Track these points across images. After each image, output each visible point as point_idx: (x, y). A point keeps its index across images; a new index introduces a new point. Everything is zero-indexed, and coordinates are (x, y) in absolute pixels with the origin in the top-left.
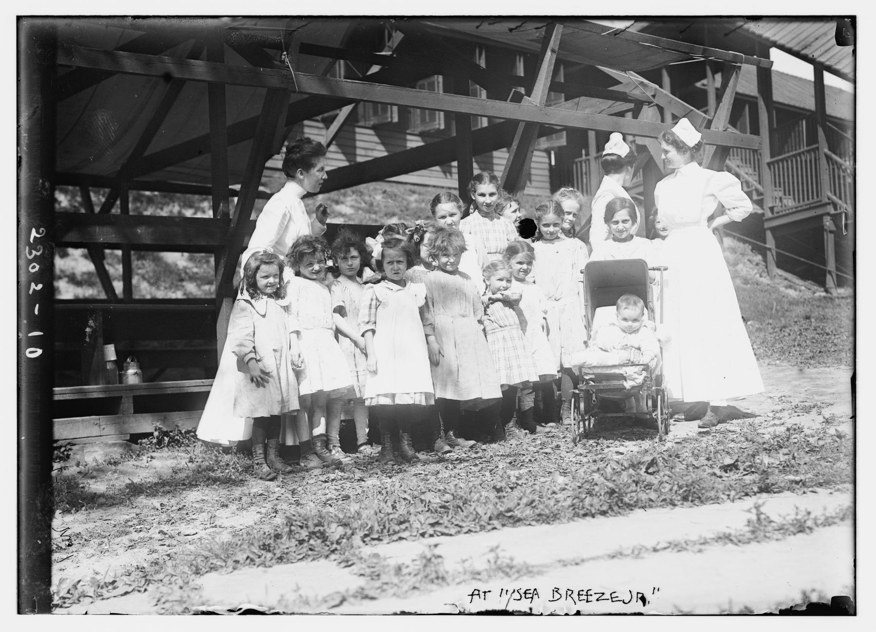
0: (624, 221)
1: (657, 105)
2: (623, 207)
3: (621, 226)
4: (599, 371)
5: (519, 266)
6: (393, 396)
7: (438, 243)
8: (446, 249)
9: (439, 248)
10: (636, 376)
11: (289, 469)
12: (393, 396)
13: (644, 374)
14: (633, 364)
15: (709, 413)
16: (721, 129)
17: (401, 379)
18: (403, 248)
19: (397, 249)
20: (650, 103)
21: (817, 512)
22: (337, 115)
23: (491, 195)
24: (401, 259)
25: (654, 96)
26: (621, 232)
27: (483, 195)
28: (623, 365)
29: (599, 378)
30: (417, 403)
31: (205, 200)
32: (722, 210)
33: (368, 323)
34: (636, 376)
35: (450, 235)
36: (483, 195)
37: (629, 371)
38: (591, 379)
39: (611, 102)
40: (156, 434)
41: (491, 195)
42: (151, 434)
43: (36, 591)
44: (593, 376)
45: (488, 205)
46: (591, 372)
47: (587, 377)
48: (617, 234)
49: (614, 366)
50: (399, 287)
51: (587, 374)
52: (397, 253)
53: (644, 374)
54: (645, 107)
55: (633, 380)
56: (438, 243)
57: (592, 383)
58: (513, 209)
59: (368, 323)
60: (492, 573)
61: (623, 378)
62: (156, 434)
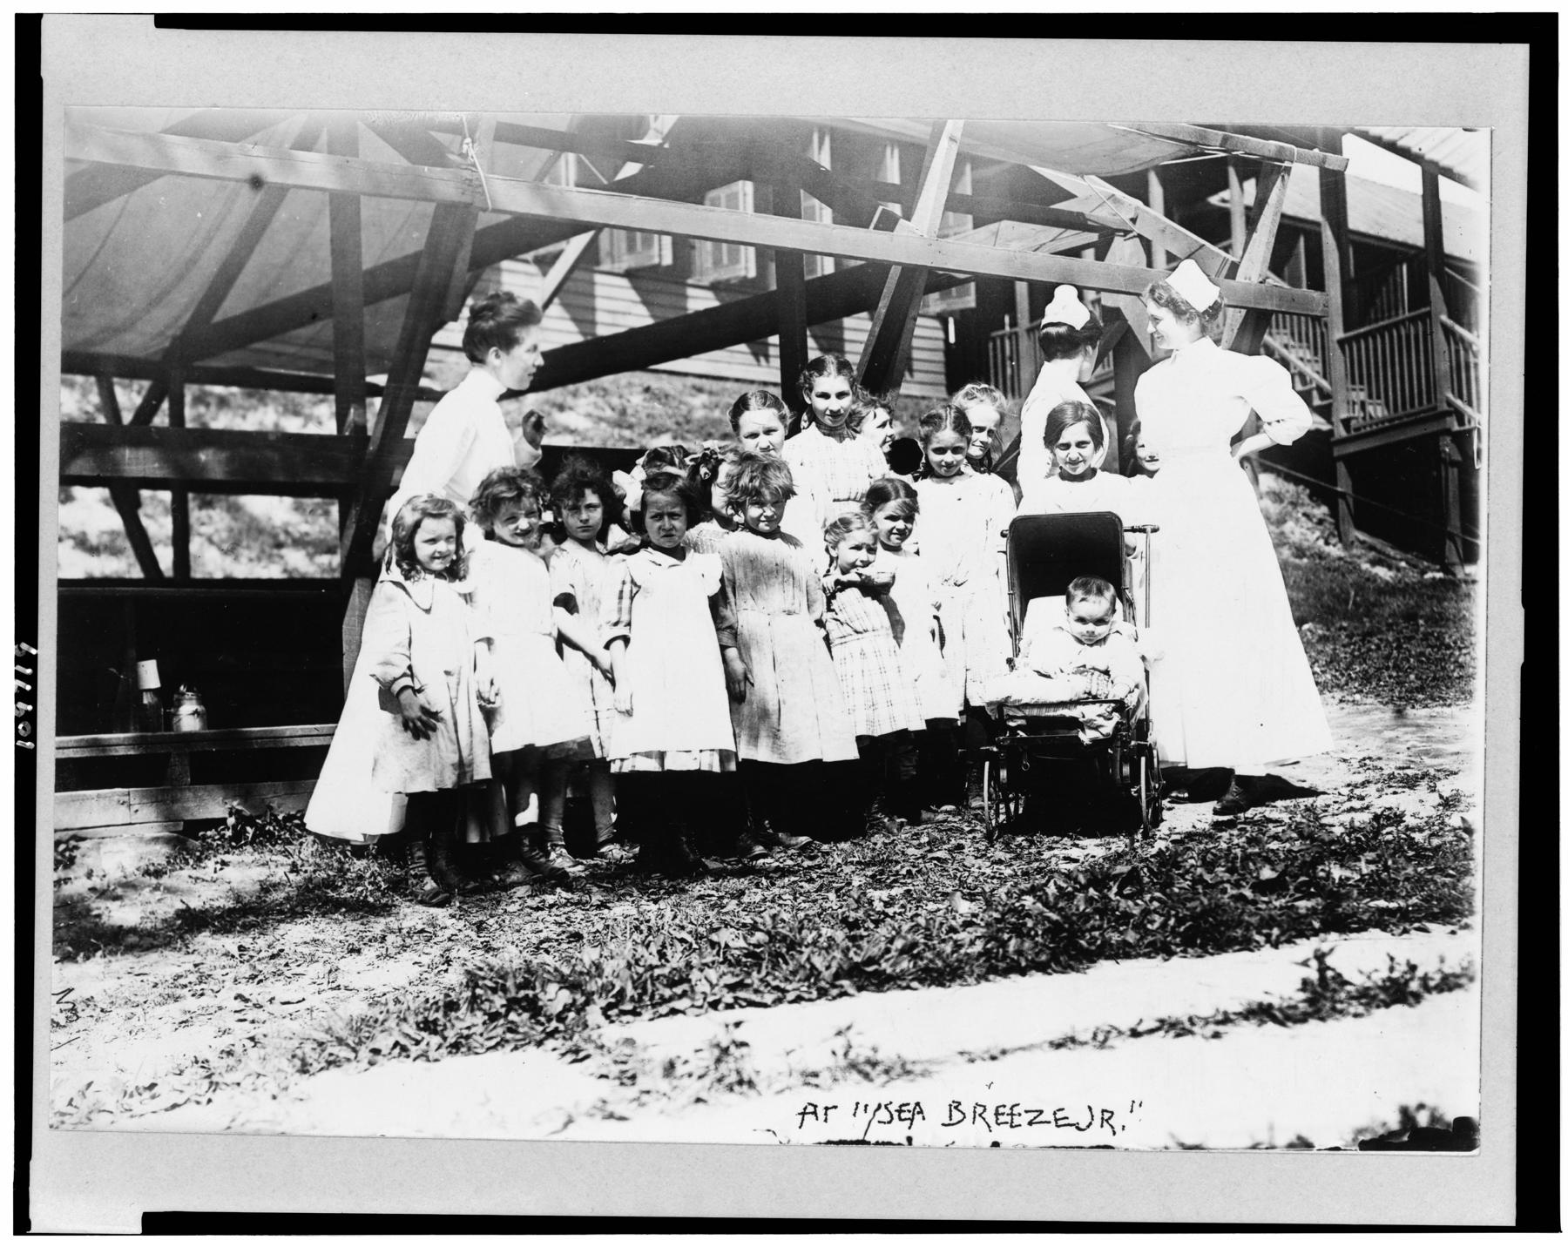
0: (1080, 444)
1: (1139, 236)
2: (1078, 419)
5: (890, 524)
6: (661, 756)
7: (745, 481)
10: (1100, 721)
23: (840, 395)
26: (1074, 463)
27: (825, 396)
29: (1034, 724)
30: (705, 768)
33: (616, 624)
34: (1100, 721)
38: (1019, 727)
40: (231, 821)
41: (840, 395)
44: (1020, 722)
45: (835, 415)
46: (1020, 714)
48: (1067, 468)
50: (673, 561)
55: (1096, 728)
59: (616, 624)
61: (1075, 724)
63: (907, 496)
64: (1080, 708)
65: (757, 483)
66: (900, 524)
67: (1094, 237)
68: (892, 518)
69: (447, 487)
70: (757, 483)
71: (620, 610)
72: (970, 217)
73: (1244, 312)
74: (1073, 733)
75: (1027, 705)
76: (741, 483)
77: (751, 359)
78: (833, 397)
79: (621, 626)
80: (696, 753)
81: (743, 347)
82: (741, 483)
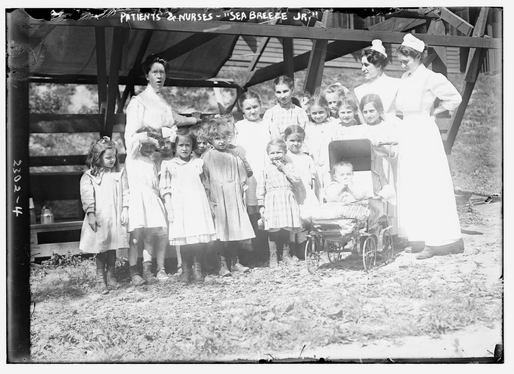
0: (371, 111)
1: (442, 19)
2: (370, 101)
3: (369, 114)
4: (323, 222)
5: (292, 143)
6: (185, 239)
7: (211, 130)
8: (217, 134)
9: (212, 135)
10: (347, 226)
11: (118, 285)
12: (185, 239)
13: (353, 225)
14: (346, 218)
15: (426, 248)
16: (479, 35)
17: (191, 225)
18: (190, 135)
19: (185, 136)
20: (436, 18)
21: (425, 338)
22: (467, 21)
23: (285, 91)
24: (189, 143)
25: (440, 13)
26: (370, 118)
27: (279, 92)
28: (339, 219)
29: (324, 227)
30: (202, 242)
31: (277, 82)
32: (437, 103)
33: (166, 188)
34: (347, 226)
35: (218, 124)
36: (279, 92)
37: (341, 223)
38: (318, 228)
39: (414, 19)
40: (53, 257)
41: (285, 91)
42: (50, 257)
43: (20, 345)
44: (319, 226)
45: (284, 99)
46: (317, 223)
47: (315, 226)
48: (368, 120)
49: (331, 219)
50: (184, 162)
51: (316, 224)
52: (187, 139)
53: (353, 225)
54: (433, 22)
55: (346, 229)
56: (211, 130)
57: (320, 231)
58: (306, 102)
59: (166, 188)
60: (422, 313)
61: (338, 227)
62: (53, 257)
63: (299, 132)
64: (339, 221)
65: (216, 131)
66: (296, 143)
67: (424, 21)
68: (292, 141)
69: (276, 104)
70: (216, 131)
71: (166, 182)
72: (317, 22)
73: (475, 49)
74: (338, 231)
75: (319, 220)
76: (210, 132)
77: (354, 60)
78: (282, 93)
79: (167, 189)
80: (198, 237)
81: (350, 55)
82: (210, 132)
